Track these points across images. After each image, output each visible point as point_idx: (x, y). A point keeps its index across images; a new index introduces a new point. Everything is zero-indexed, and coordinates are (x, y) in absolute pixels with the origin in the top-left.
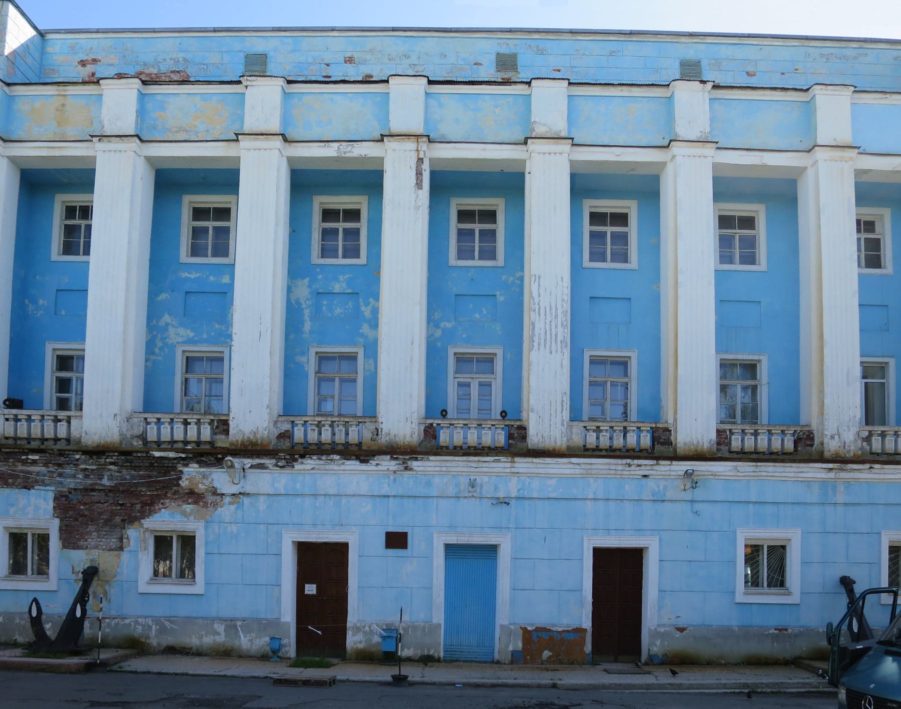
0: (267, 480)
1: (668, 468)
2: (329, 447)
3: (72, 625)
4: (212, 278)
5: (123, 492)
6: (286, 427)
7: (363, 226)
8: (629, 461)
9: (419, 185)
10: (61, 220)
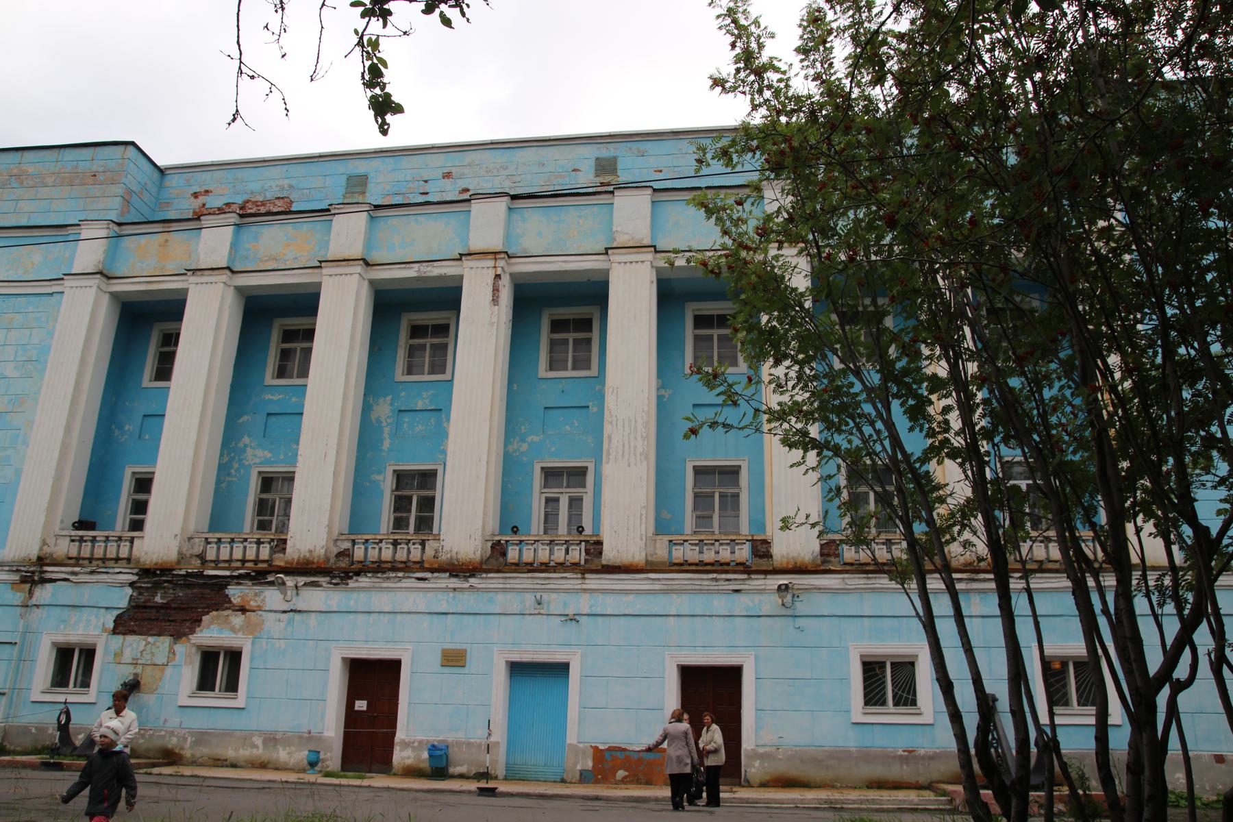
0: (319, 597)
1: (762, 582)
2: (389, 565)
4: (294, 399)
6: (347, 545)
7: (595, 334)
8: (715, 575)
9: (495, 301)
10: (157, 347)
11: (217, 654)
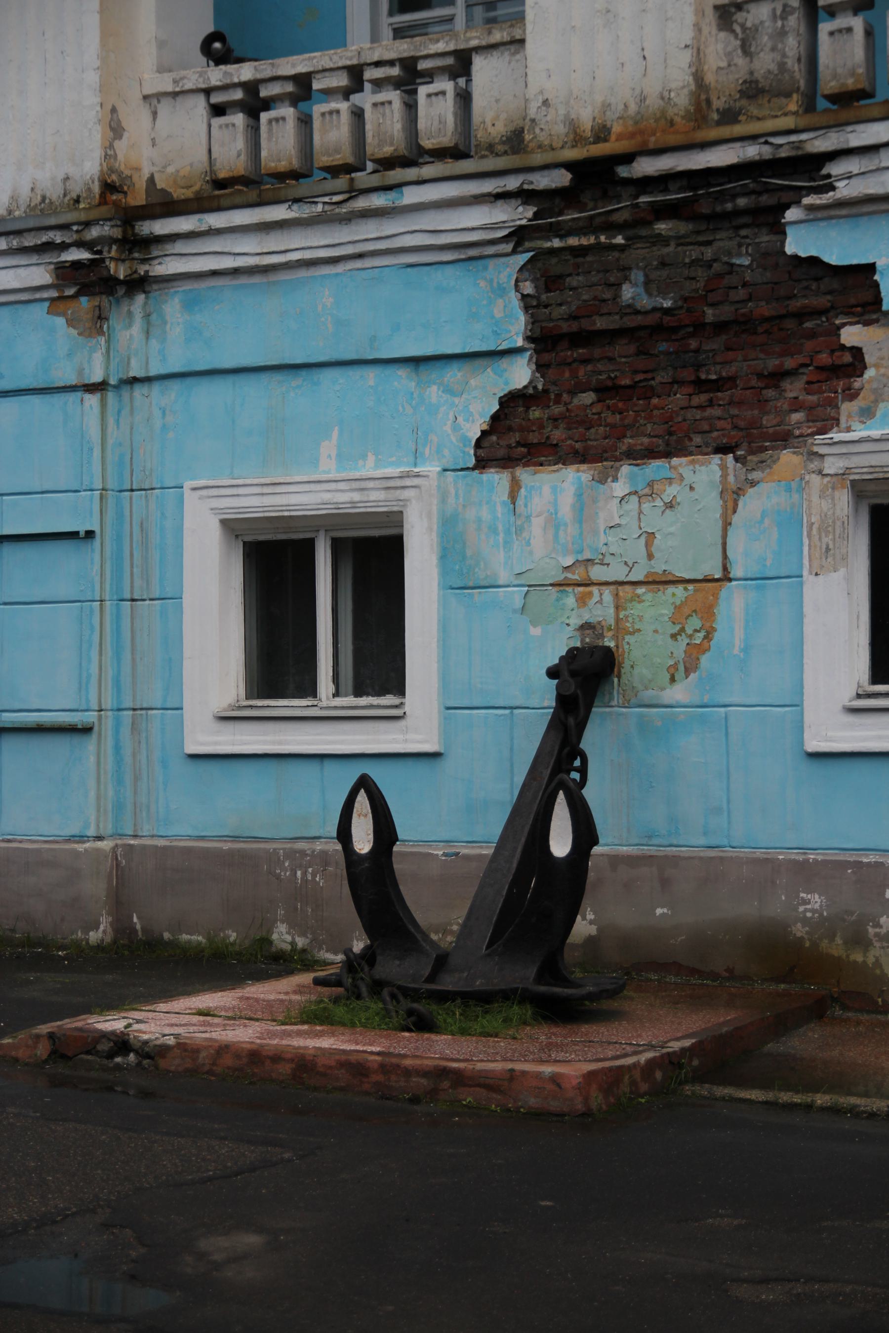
3: (537, 888)
5: (720, 327)
11: (304, 551)
